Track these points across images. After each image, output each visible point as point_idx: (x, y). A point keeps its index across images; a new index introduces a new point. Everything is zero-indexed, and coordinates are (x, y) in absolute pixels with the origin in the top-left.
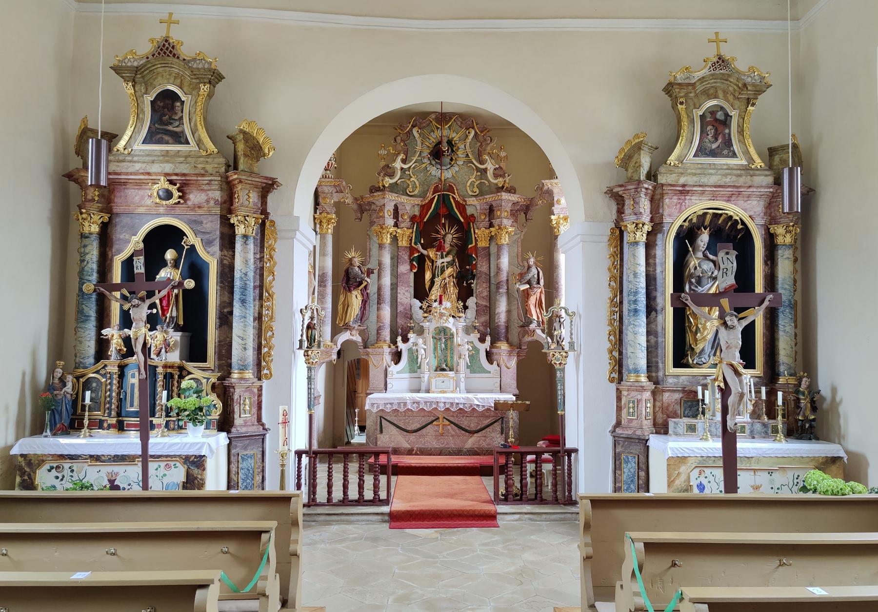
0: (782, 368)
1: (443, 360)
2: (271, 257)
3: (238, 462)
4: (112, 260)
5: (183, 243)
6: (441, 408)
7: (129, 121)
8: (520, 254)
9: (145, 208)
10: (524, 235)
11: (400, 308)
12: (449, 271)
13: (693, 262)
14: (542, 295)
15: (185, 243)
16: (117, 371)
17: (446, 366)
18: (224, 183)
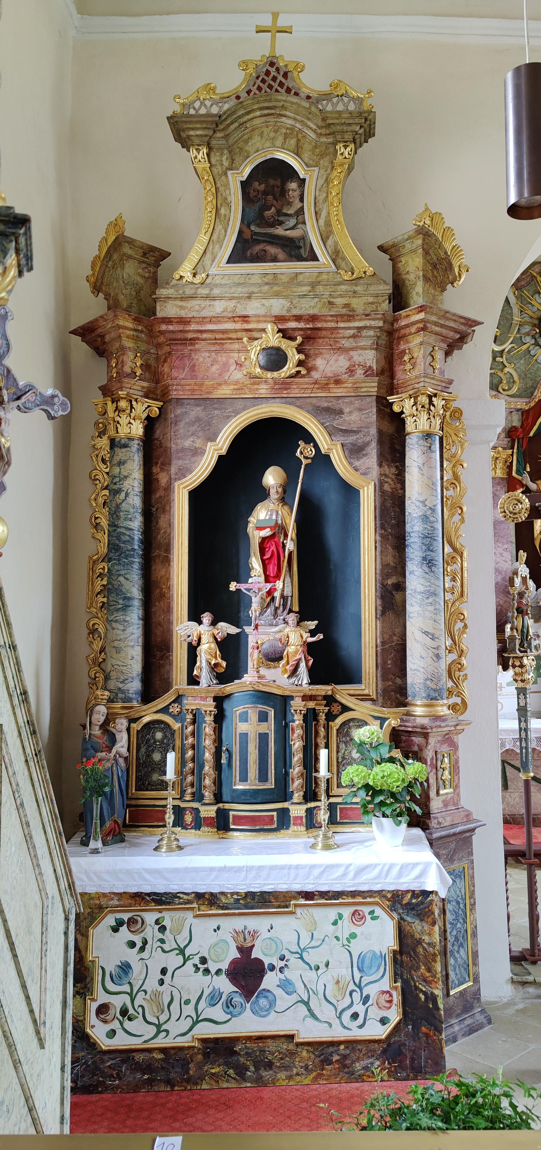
2: (456, 477)
4: (169, 489)
5: (298, 454)
9: (232, 387)
15: (301, 453)
16: (212, 709)
18: (385, 334)
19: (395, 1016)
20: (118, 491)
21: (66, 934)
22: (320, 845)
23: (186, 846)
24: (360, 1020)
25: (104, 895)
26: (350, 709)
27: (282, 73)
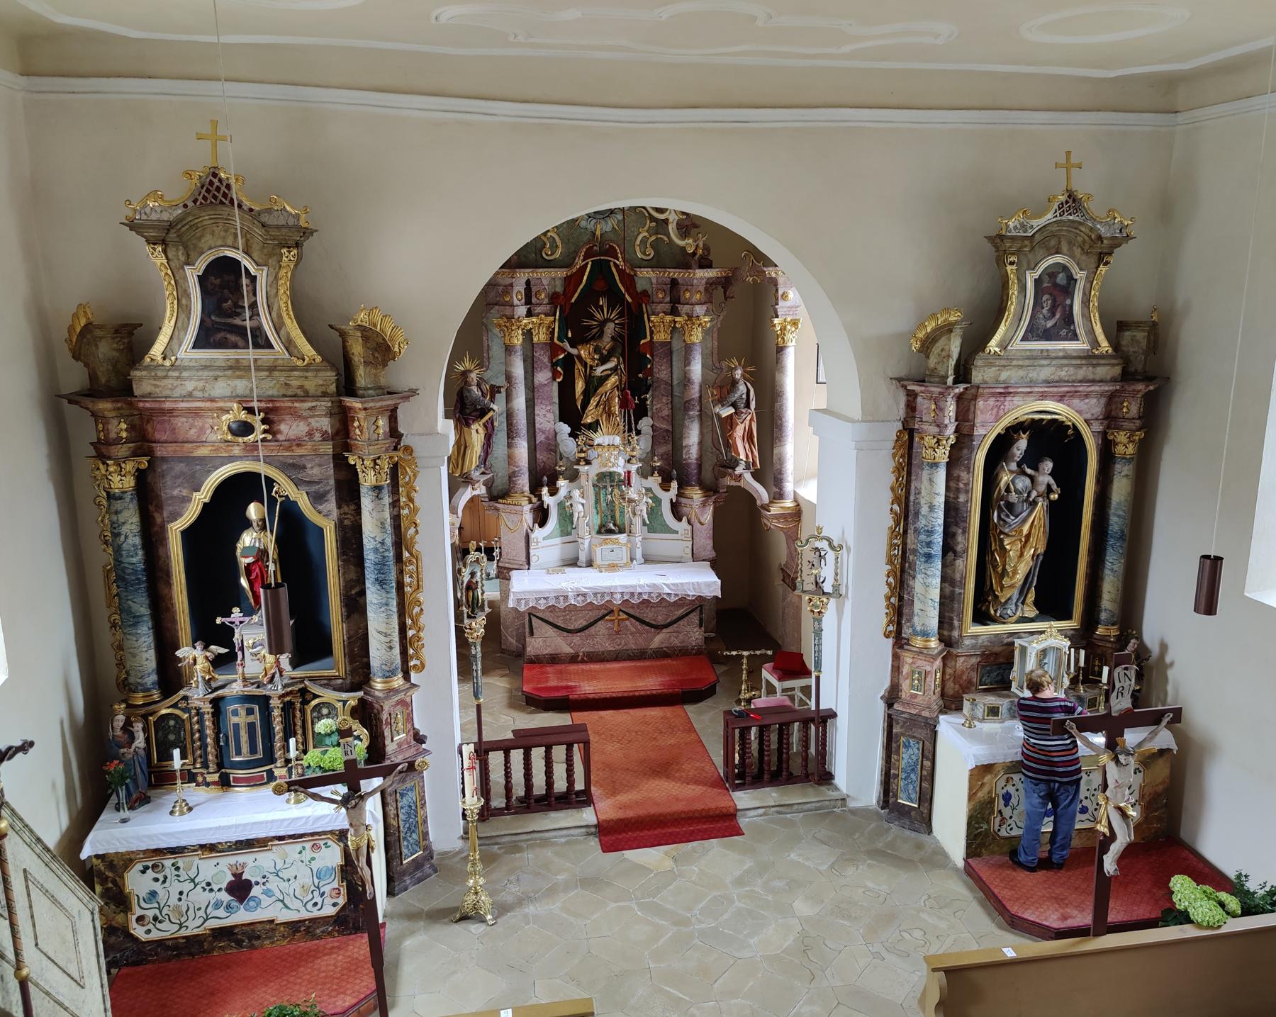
0: (1103, 616)
1: (609, 517)
2: (411, 500)
3: (397, 801)
4: (163, 529)
6: (618, 600)
7: (165, 311)
8: (716, 351)
9: (210, 448)
10: (722, 321)
11: (540, 438)
12: (613, 379)
13: (1005, 478)
14: (753, 423)
17: (615, 525)
19: (342, 901)
20: (119, 535)
21: (93, 921)
22: (293, 801)
23: (196, 806)
24: (319, 906)
25: (133, 852)
26: (319, 696)
27: (225, 184)
